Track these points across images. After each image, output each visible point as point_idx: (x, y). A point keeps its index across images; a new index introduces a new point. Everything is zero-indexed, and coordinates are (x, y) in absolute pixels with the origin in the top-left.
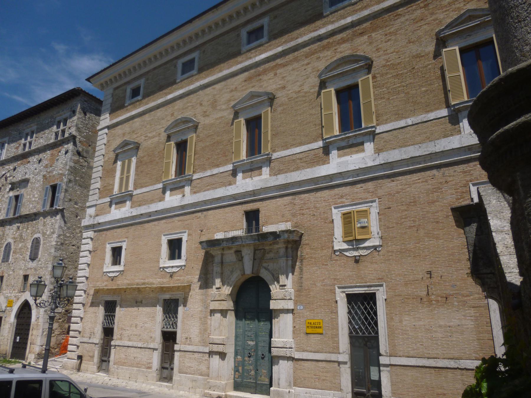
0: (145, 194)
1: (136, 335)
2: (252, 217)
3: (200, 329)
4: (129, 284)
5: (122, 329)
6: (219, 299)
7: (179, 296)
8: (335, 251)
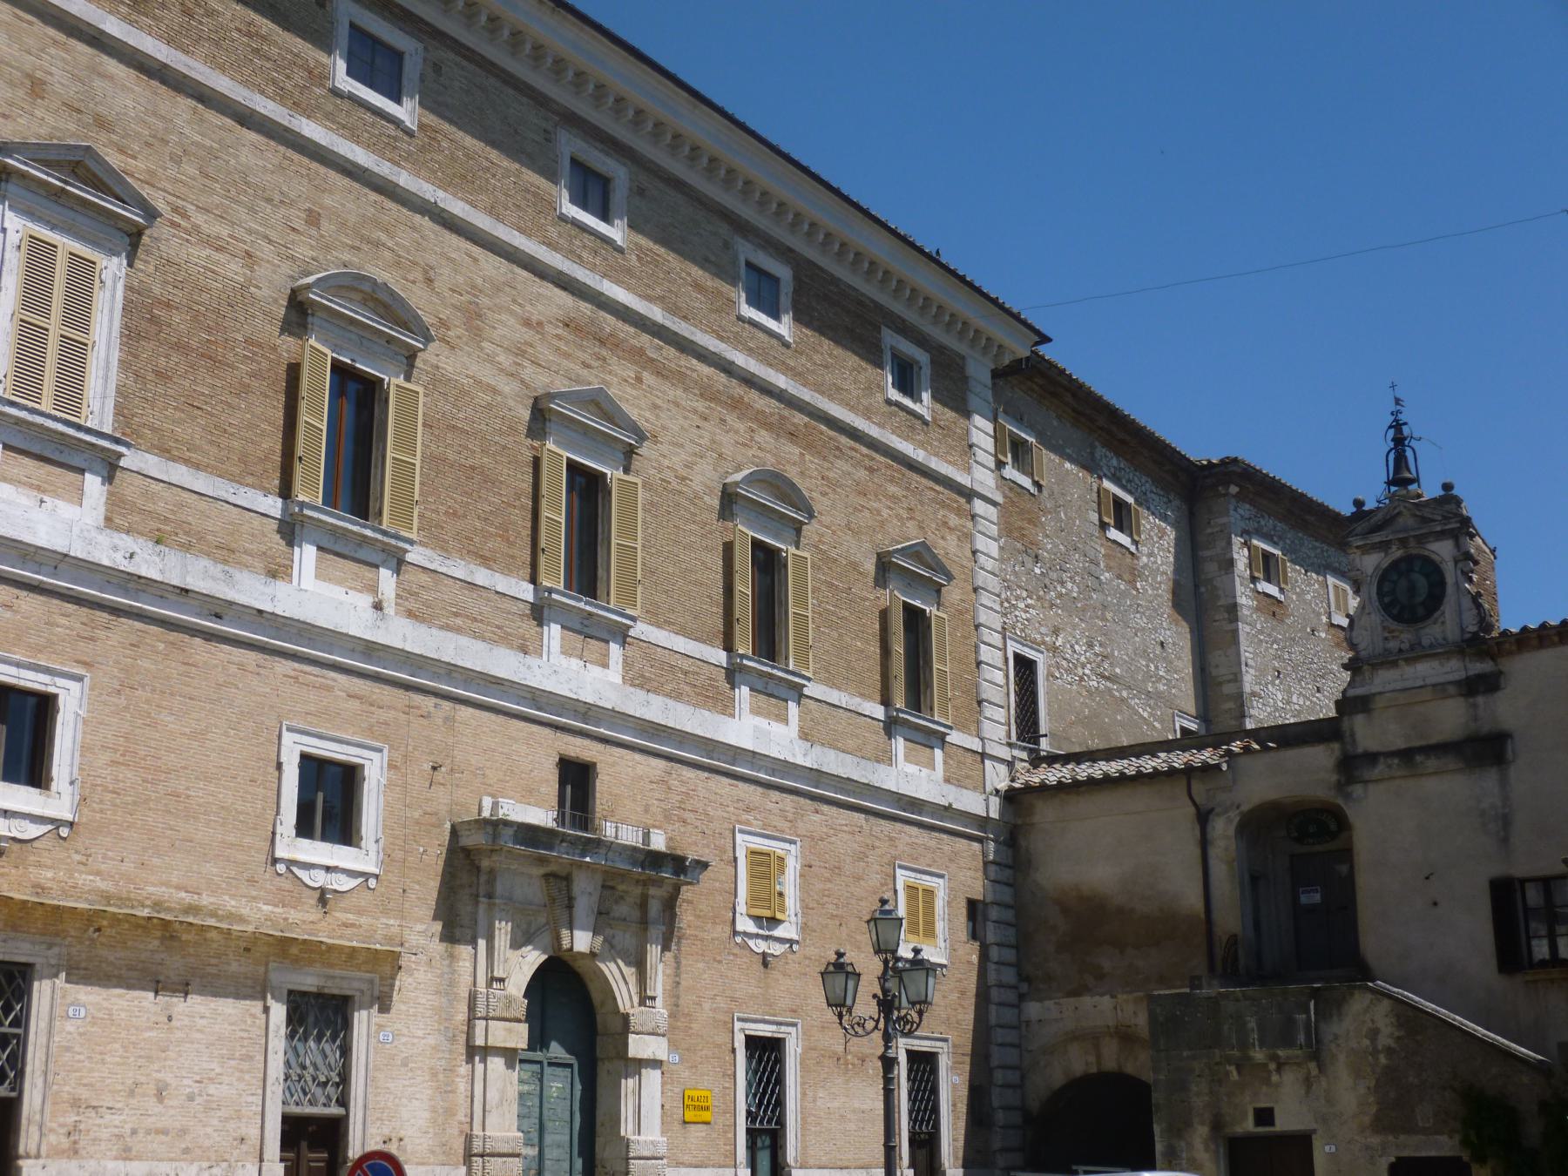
0: (186, 495)
1: (165, 1132)
2: (576, 780)
3: (433, 1110)
4: (107, 898)
5: (76, 1103)
6: (507, 1015)
7: (356, 985)
8: (275, 861)
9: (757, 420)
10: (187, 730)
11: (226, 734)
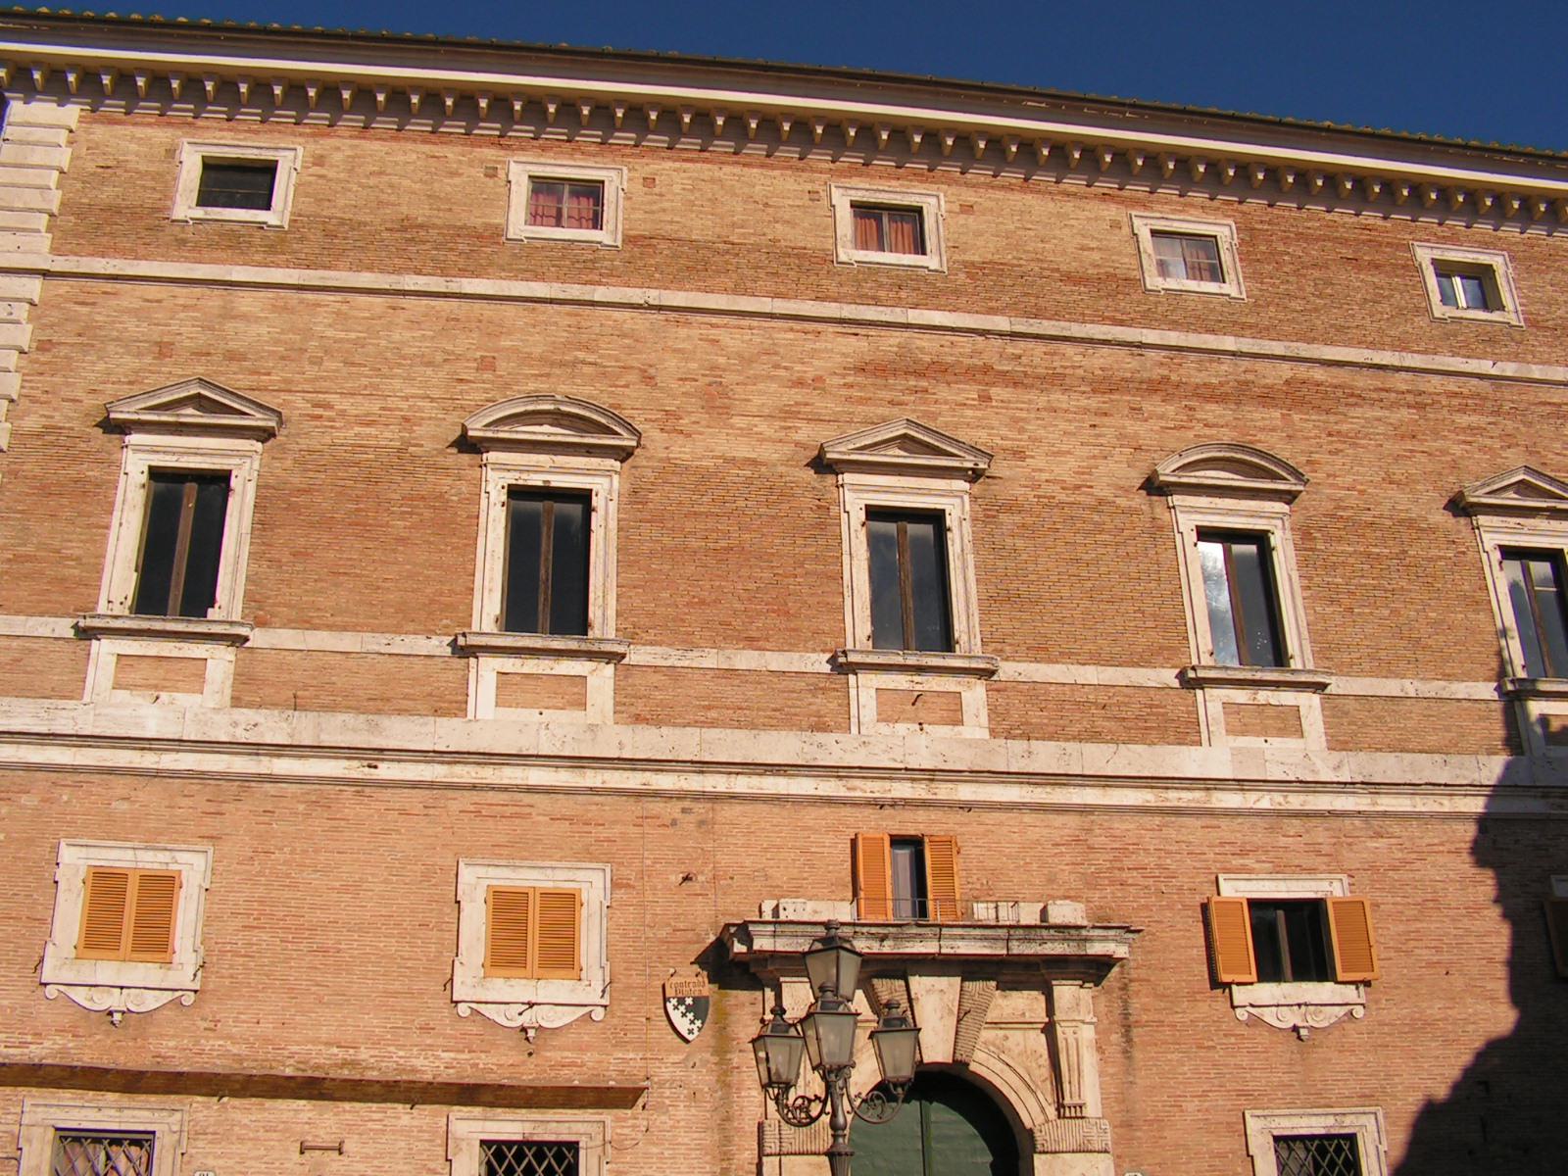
7: (582, 1128)
9: (1198, 396)
10: (337, 884)
11: (386, 881)
